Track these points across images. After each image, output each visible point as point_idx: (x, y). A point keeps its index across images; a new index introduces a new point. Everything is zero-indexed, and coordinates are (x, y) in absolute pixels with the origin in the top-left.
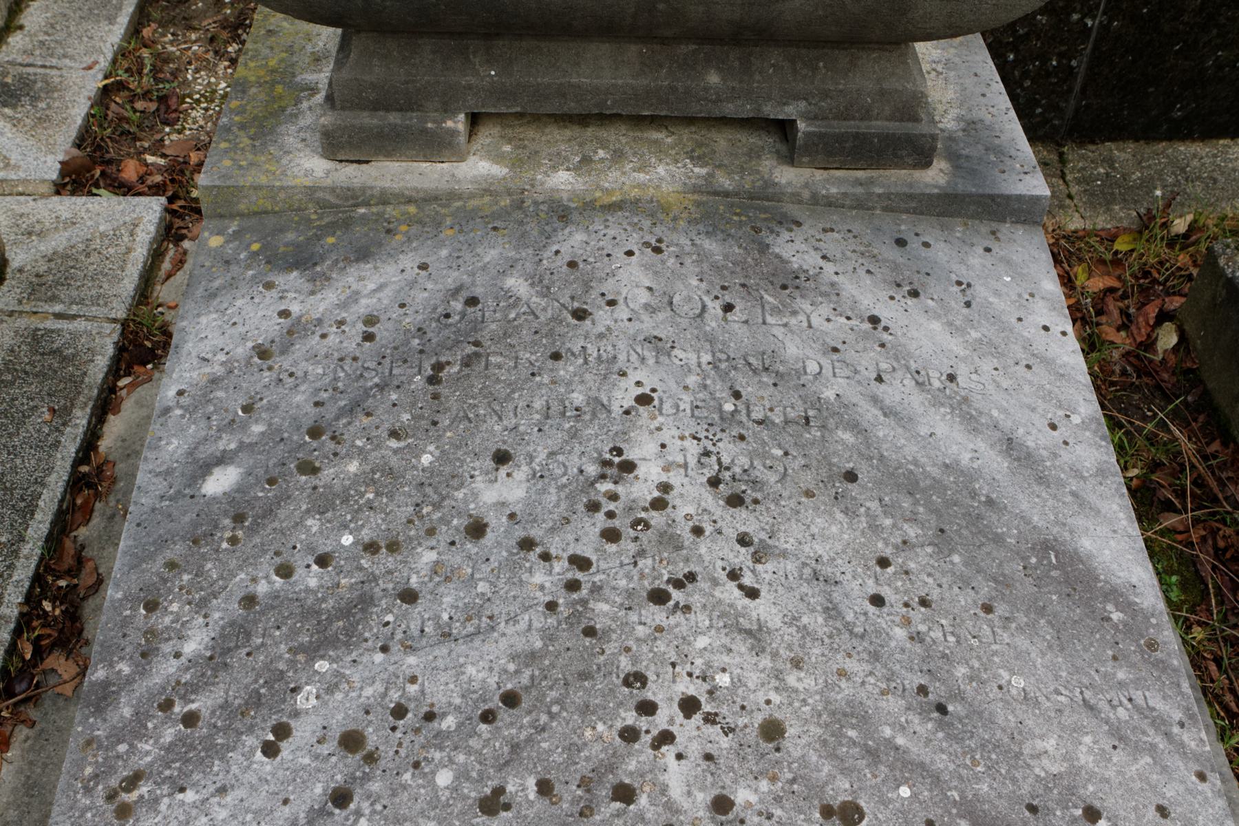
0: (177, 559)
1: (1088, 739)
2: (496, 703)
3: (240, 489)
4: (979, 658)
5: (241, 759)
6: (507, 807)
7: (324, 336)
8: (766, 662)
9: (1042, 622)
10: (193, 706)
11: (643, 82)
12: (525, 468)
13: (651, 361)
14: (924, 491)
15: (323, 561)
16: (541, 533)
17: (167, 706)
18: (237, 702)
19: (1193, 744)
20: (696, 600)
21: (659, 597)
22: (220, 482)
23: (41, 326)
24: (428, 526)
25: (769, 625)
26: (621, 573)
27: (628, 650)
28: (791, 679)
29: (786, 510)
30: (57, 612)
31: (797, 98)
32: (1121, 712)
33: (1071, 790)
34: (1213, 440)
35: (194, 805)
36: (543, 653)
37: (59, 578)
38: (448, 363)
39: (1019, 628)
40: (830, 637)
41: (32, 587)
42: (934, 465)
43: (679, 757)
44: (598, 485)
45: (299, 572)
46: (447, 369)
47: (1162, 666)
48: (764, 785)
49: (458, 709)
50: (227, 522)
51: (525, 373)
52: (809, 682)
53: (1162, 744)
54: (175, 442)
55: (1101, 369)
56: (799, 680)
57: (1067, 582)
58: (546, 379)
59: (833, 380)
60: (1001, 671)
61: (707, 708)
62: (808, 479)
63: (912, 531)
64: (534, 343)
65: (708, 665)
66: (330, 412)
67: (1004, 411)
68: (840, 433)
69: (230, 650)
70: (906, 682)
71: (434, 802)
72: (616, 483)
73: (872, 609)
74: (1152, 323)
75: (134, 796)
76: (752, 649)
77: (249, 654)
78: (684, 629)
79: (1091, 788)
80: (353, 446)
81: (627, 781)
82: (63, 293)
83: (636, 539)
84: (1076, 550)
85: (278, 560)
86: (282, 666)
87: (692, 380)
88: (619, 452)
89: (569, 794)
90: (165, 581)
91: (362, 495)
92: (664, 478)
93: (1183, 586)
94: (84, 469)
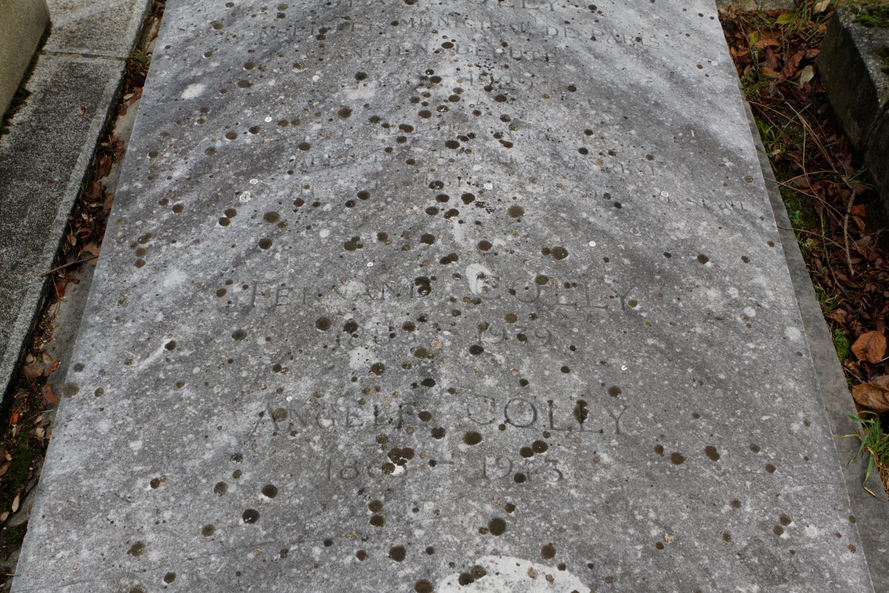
0: (168, 131)
1: (705, 224)
2: (355, 197)
3: (204, 95)
4: (643, 182)
5: (207, 227)
6: (360, 246)
7: (254, 16)
8: (514, 179)
9: (683, 165)
10: (179, 202)
12: (375, 81)
13: (453, 26)
14: (616, 97)
15: (254, 130)
16: (383, 114)
17: (164, 202)
18: (204, 200)
19: (768, 229)
20: (475, 147)
21: (452, 145)
22: (192, 93)
23: (75, 61)
24: (316, 111)
25: (518, 161)
26: (430, 133)
27: (433, 170)
28: (529, 188)
29: (532, 104)
30: (91, 220)
32: (726, 211)
33: (692, 247)
34: (832, 134)
35: (181, 249)
36: (383, 173)
37: (92, 202)
38: (329, 28)
39: (669, 168)
40: (554, 168)
41: (75, 206)
42: (624, 84)
43: (461, 222)
44: (418, 90)
45: (240, 136)
46: (329, 31)
47: (755, 190)
48: (510, 237)
49: (333, 201)
50: (197, 112)
51: (375, 32)
52: (540, 190)
53: (749, 227)
54: (165, 73)
55: (760, 92)
56: (534, 188)
57: (700, 146)
58: (388, 36)
59: (564, 38)
60: (656, 189)
61: (478, 199)
62: (545, 89)
63: (607, 118)
64: (382, 17)
65: (480, 179)
66: (258, 55)
67: (671, 58)
68: (567, 66)
69: (200, 175)
70: (598, 192)
71: (319, 244)
72: (429, 88)
73: (579, 155)
74: (797, 65)
75: (146, 245)
76: (507, 172)
77: (211, 177)
78: (466, 161)
79: (704, 247)
80: (272, 72)
81: (430, 233)
82: (88, 43)
83: (440, 116)
84: (707, 131)
85: (228, 130)
86: (230, 182)
87: (477, 36)
88: (432, 72)
89: (396, 240)
90: (161, 142)
91: (277, 97)
92: (458, 86)
93: (805, 218)
94: (105, 144)
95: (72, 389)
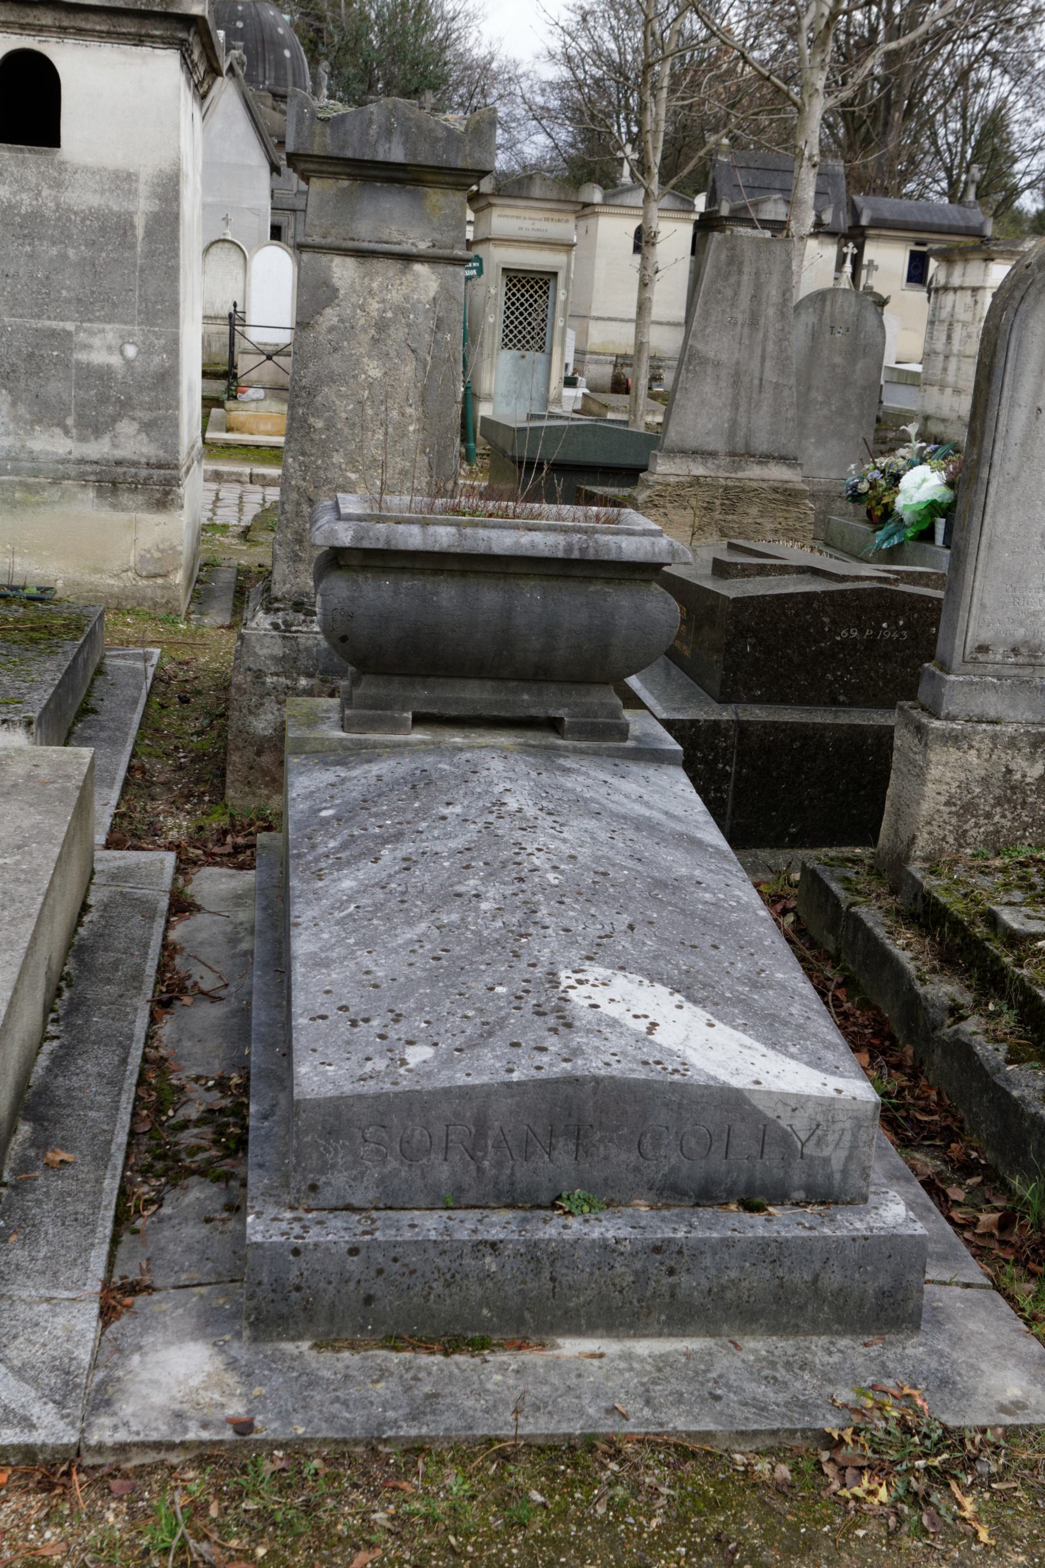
11: (494, 697)
31: (564, 706)
95: (297, 925)
